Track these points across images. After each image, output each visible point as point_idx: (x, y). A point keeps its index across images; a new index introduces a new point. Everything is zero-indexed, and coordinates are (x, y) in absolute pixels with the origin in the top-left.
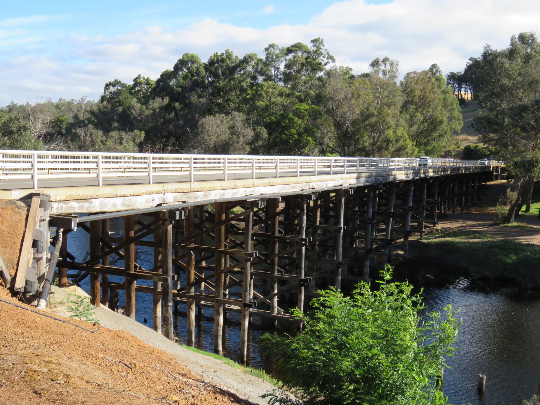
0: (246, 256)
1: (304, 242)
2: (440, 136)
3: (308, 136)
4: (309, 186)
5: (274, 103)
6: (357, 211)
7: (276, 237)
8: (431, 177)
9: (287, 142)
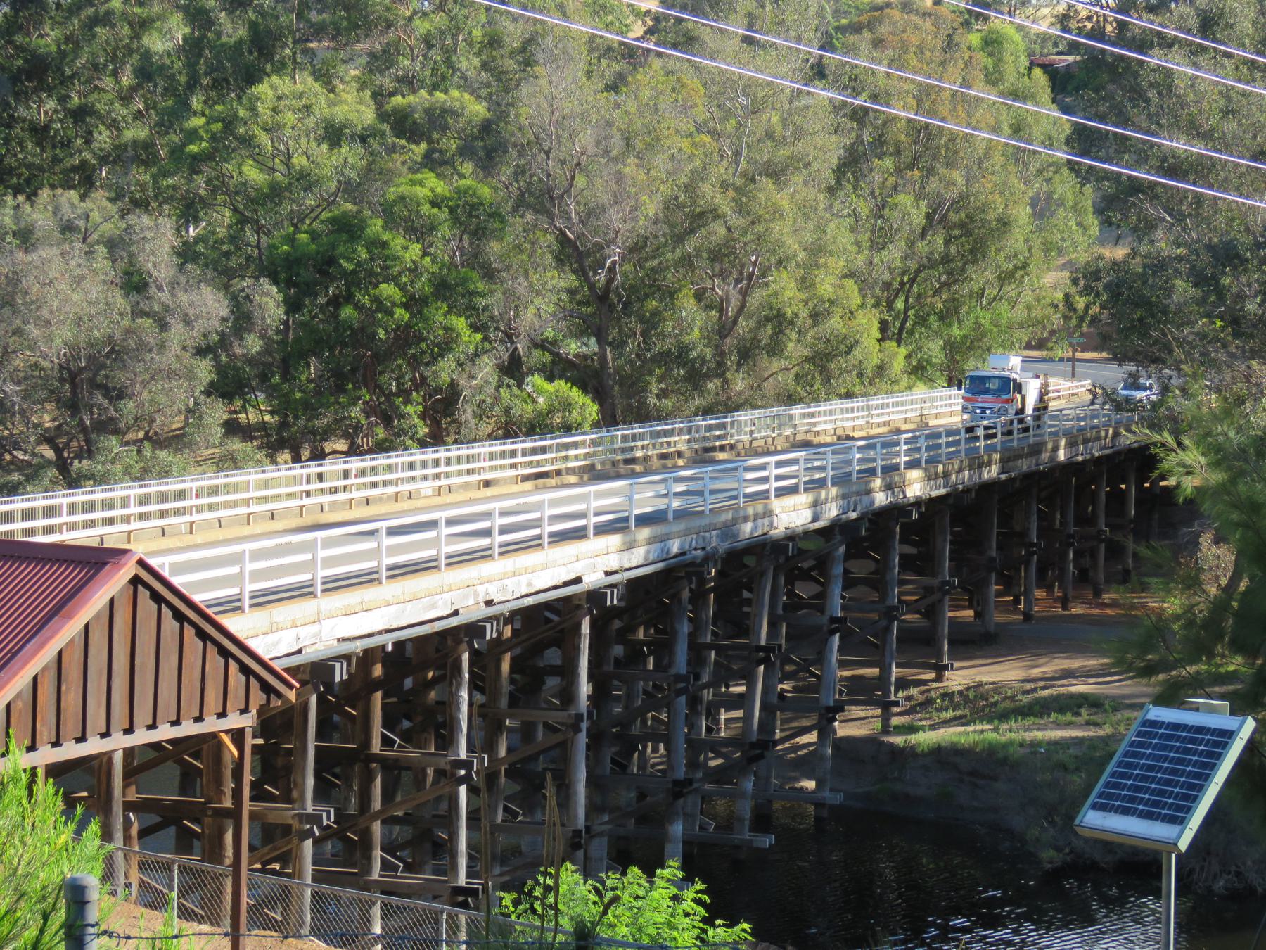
0: (301, 822)
1: (463, 772)
2: (1005, 277)
3: (449, 312)
4: (476, 594)
5: (303, 175)
6: (642, 643)
7: (375, 758)
8: (918, 503)
9: (362, 336)
